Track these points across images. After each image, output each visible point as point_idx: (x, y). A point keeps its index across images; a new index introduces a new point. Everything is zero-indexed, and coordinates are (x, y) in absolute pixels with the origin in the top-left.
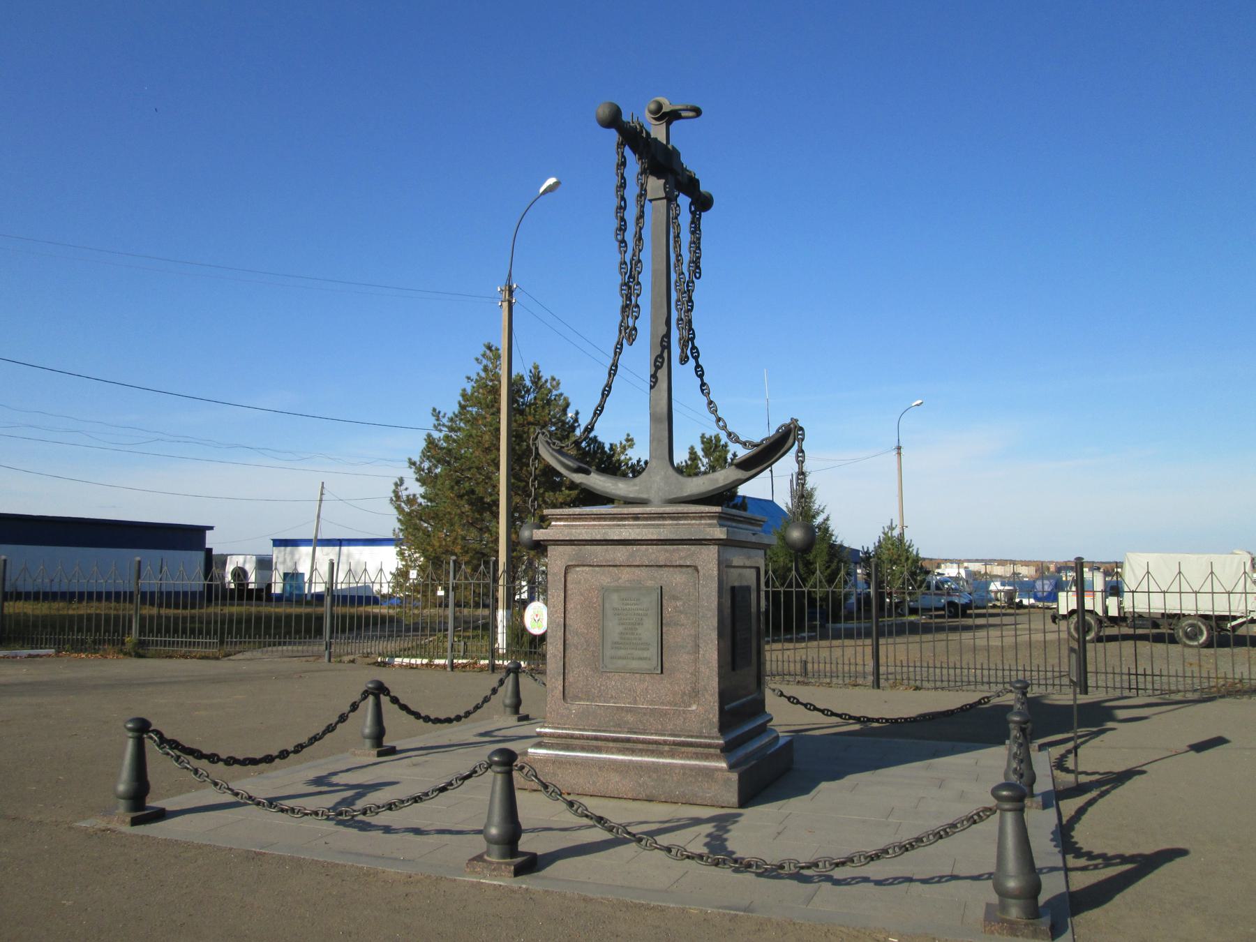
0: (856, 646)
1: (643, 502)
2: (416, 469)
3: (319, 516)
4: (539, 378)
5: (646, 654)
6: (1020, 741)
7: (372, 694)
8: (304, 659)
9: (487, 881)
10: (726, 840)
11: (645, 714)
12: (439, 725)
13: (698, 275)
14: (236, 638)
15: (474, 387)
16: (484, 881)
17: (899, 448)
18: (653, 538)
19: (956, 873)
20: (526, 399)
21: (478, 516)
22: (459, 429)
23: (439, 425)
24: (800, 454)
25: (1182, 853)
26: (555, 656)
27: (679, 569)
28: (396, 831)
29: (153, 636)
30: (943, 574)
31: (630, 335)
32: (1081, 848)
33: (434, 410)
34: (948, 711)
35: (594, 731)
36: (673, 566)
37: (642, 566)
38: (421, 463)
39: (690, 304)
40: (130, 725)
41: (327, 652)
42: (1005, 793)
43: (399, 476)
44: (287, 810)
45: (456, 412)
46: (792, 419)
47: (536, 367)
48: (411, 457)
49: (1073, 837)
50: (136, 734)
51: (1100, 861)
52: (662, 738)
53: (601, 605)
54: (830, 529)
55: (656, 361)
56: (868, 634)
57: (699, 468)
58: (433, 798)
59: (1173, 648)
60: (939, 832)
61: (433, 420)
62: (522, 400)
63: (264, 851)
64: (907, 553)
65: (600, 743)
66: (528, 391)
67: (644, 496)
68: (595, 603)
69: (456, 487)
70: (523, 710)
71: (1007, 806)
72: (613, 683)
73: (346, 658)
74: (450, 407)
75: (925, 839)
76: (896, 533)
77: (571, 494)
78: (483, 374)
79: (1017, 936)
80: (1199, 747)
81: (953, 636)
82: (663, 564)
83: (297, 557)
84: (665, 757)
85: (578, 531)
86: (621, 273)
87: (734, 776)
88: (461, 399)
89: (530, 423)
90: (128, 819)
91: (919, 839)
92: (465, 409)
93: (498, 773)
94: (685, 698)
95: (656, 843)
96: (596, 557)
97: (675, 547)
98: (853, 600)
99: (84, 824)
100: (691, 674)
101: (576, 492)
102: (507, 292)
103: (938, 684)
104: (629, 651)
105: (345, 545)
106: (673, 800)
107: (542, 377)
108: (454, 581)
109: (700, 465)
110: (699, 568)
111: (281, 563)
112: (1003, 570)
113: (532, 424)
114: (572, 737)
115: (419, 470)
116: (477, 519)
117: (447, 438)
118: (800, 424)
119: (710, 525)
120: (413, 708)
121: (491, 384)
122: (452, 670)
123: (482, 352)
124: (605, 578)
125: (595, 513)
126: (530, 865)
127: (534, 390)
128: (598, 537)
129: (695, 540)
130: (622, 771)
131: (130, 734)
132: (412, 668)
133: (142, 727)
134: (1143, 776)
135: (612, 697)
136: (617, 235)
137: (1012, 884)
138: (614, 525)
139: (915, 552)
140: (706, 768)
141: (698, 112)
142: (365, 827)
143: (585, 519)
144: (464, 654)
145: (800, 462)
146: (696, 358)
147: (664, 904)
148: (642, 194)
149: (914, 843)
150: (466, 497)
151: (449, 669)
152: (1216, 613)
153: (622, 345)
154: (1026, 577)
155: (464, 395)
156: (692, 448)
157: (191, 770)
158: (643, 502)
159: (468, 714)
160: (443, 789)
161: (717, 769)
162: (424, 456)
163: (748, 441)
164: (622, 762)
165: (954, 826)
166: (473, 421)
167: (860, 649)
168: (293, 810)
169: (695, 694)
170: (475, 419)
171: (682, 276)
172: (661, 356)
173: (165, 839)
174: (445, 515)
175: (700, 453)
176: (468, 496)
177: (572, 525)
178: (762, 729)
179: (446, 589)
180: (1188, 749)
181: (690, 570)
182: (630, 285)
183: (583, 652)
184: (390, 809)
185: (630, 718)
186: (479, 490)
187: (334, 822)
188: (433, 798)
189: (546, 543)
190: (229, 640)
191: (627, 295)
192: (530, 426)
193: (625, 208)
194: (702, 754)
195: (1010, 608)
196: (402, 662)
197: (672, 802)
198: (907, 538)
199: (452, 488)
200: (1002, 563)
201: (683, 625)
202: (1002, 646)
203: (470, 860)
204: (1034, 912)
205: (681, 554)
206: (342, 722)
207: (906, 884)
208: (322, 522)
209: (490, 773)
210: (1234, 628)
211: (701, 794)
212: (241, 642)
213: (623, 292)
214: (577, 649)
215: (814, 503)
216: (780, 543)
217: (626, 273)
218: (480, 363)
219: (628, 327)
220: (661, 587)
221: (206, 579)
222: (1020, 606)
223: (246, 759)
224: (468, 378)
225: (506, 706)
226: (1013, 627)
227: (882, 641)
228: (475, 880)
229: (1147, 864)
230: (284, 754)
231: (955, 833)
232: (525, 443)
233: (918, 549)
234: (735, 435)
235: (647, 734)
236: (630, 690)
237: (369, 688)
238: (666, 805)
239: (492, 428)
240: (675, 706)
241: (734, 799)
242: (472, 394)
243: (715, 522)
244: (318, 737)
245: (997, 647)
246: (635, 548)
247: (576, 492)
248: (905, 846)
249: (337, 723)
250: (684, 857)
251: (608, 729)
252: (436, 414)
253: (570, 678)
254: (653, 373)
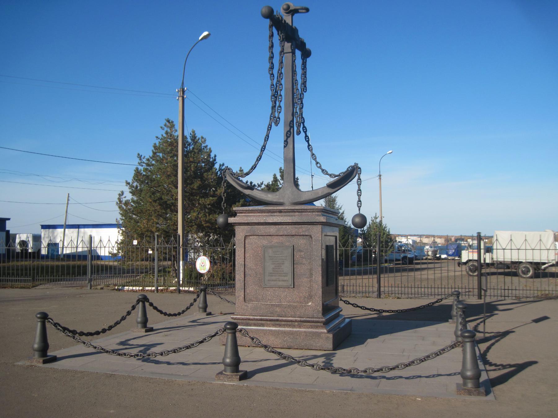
0: (369, 278)
1: (281, 204)
2: (129, 186)
3: (67, 212)
4: (195, 138)
5: (285, 278)
6: (462, 316)
7: (141, 301)
8: (75, 288)
9: (227, 383)
10: (332, 364)
11: (285, 307)
12: (171, 317)
13: (305, 90)
14: (41, 277)
15: (160, 142)
16: (226, 383)
17: (380, 176)
18: (289, 221)
19: (439, 373)
20: (188, 149)
21: (164, 212)
22: (153, 165)
23: (141, 162)
24: (359, 181)
25: (535, 362)
26: (240, 280)
27: (302, 236)
28: (173, 364)
29: (5, 277)
30: (402, 242)
31: (277, 121)
32: (491, 362)
33: (139, 154)
34: (412, 308)
35: (260, 316)
36: (299, 235)
37: (284, 235)
38: (133, 183)
39: (302, 105)
40: (38, 316)
41: (89, 284)
42: (466, 334)
43: (121, 190)
44: (122, 355)
45: (151, 156)
46: (355, 163)
47: (194, 132)
48: (127, 180)
49: (487, 358)
50: (42, 320)
51: (500, 367)
52: (295, 319)
53: (263, 255)
54: (344, 218)
55: (287, 133)
56: (375, 273)
57: (279, 186)
58: (196, 346)
59: (515, 279)
60: (437, 353)
61: (138, 160)
62: (186, 149)
63: (113, 373)
64: (384, 231)
65: (263, 322)
66: (189, 145)
67: (282, 201)
68: (260, 254)
69: (153, 196)
70: (208, 310)
71: (467, 340)
72: (269, 293)
73: (99, 287)
74: (148, 153)
75: (431, 356)
76: (378, 220)
77: (214, 199)
78: (165, 135)
79: (471, 395)
80: (537, 321)
81: (412, 274)
82: (294, 234)
83: (55, 234)
84: (296, 328)
85: (252, 218)
86: (271, 90)
87: (331, 336)
88: (153, 148)
89: (191, 162)
90: (41, 361)
91: (428, 356)
92: (156, 154)
93: (230, 333)
94: (305, 299)
95: (307, 363)
96: (260, 231)
97: (300, 226)
98: (355, 256)
99: (20, 363)
100: (309, 288)
101: (216, 198)
102: (181, 92)
103: (410, 296)
104: (278, 277)
105: (81, 228)
106: (301, 348)
107: (197, 136)
108: (158, 246)
109: (279, 184)
110: (312, 236)
111: (47, 238)
112: (428, 240)
113: (192, 162)
114: (249, 319)
115: (132, 187)
116: (164, 213)
117: (146, 170)
118: (359, 166)
119: (318, 215)
120: (159, 308)
121: (169, 140)
122: (157, 292)
123: (164, 124)
124: (265, 242)
125: (260, 209)
126: (245, 376)
127: (193, 144)
128: (262, 221)
129: (310, 222)
130: (275, 335)
131: (39, 320)
132: (134, 292)
133: (44, 317)
134: (513, 334)
135: (269, 300)
136: (269, 71)
137: (469, 373)
138: (269, 215)
139: (387, 231)
140: (317, 332)
141: (307, 10)
142: (157, 362)
143: (255, 212)
144: (164, 284)
145: (359, 185)
146: (305, 132)
147: (313, 389)
148: (282, 52)
149: (426, 358)
150: (158, 201)
151: (155, 292)
152: (535, 261)
153: (271, 126)
154: (440, 244)
155: (155, 147)
156: (275, 175)
157: (71, 337)
158: (281, 204)
159: (183, 312)
160: (201, 342)
161: (322, 333)
162: (134, 180)
163: (332, 174)
164: (275, 331)
165: (443, 350)
166: (161, 161)
167: (371, 280)
168: (125, 354)
169: (310, 297)
170: (162, 159)
171: (297, 91)
172: (289, 131)
173: (63, 369)
174: (146, 211)
175: (279, 178)
176: (159, 200)
177: (248, 216)
178: (337, 315)
179: (153, 250)
180: (532, 321)
181: (308, 237)
182: (275, 96)
183: (254, 278)
184: (175, 352)
185: (278, 309)
186: (165, 198)
187: (141, 361)
188: (196, 346)
189: (234, 224)
190: (37, 278)
191: (274, 101)
192: (191, 163)
193: (273, 57)
194: (314, 326)
195: (434, 259)
196: (129, 289)
197: (300, 349)
198: (384, 223)
199: (150, 196)
200: (428, 236)
201: (304, 264)
202: (434, 278)
203: (217, 374)
204: (478, 385)
205: (303, 229)
206: (129, 315)
207: (419, 379)
208: (68, 215)
209: (225, 334)
210: (545, 269)
211: (315, 344)
212: (43, 279)
213: (272, 99)
214: (251, 277)
215: (336, 204)
216: (201, 235)
217: (274, 90)
218: (163, 129)
219: (275, 117)
220: (293, 246)
221: (6, 246)
222: (439, 258)
223: (88, 333)
224: (157, 137)
225: (200, 308)
226: (440, 269)
227: (382, 276)
228: (221, 383)
229: (520, 367)
230: (104, 331)
231: (444, 353)
232: (189, 173)
233: (389, 229)
234: (326, 171)
235: (287, 317)
236: (278, 296)
237: (140, 298)
238: (297, 350)
239: (171, 164)
240: (300, 303)
241: (330, 346)
242: (160, 147)
243: (320, 213)
244: (118, 322)
245: (432, 279)
246: (280, 226)
247: (216, 198)
248: (422, 359)
249: (126, 316)
250: (320, 369)
251: (267, 315)
252: (140, 156)
253: (248, 291)
254: (285, 139)
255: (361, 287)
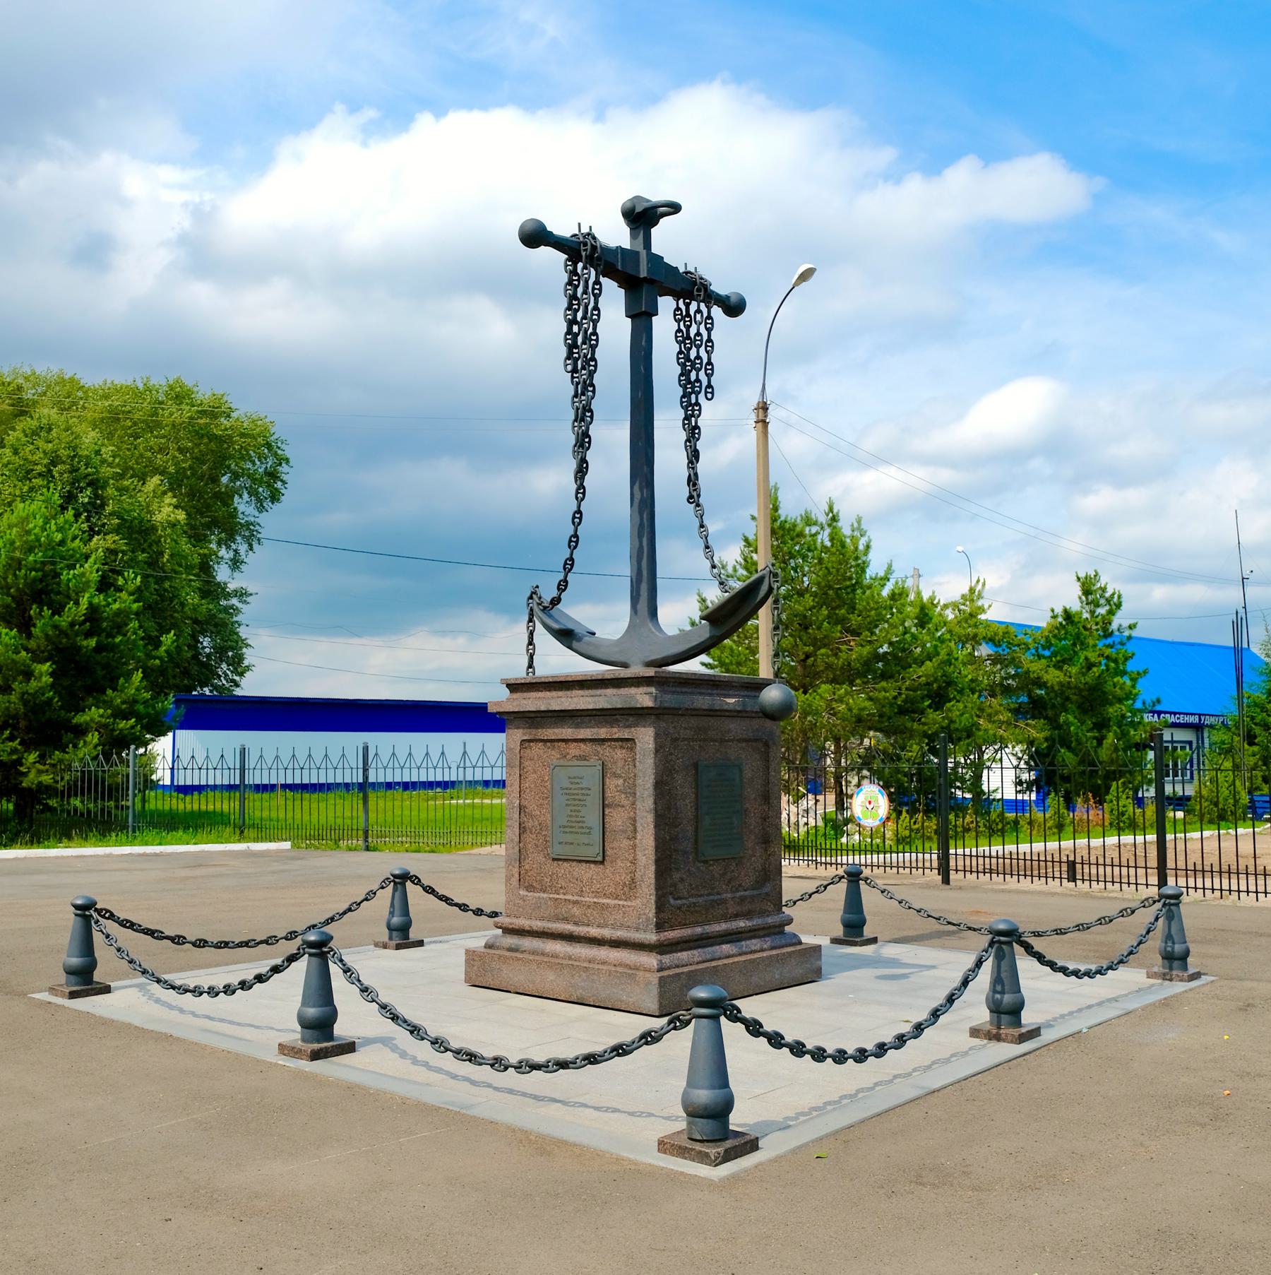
5: (585, 839)
255: (1041, 859)
